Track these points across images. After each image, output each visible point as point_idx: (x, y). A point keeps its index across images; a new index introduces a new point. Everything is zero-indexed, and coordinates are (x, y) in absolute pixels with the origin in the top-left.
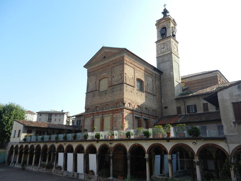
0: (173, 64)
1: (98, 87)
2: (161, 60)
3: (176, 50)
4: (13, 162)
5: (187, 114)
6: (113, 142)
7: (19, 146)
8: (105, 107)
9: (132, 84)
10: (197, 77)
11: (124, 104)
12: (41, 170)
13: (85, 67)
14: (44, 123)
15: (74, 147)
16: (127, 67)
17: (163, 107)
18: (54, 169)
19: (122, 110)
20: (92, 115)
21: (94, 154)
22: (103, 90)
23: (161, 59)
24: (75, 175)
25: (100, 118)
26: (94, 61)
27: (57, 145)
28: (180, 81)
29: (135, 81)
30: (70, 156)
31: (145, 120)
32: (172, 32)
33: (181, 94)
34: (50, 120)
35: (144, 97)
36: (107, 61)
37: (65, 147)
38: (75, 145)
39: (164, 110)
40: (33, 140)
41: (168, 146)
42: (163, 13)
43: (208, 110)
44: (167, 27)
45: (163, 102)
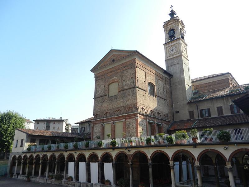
0: (184, 67)
1: (107, 92)
2: (170, 63)
3: (185, 52)
4: (17, 174)
5: (200, 118)
6: (132, 149)
7: (23, 156)
8: (116, 112)
9: (144, 88)
10: (207, 80)
11: (137, 109)
12: (49, 181)
13: (91, 71)
14: (43, 131)
15: (76, 156)
16: (139, 71)
17: (175, 111)
18: (64, 180)
19: (135, 116)
20: (102, 122)
21: (84, 162)
22: (113, 95)
23: (170, 62)
24: (89, 185)
25: (111, 124)
26: (102, 65)
27: (66, 155)
28: (191, 85)
29: (147, 84)
30: (82, 165)
31: (158, 125)
32: (181, 34)
33: (193, 98)
34: (48, 128)
35: (156, 101)
36: (116, 65)
37: (76, 156)
38: (87, 154)
39: (175, 115)
40: (37, 150)
41: (196, 152)
42: (170, 14)
43: (222, 114)
44: (175, 29)
45: (174, 106)
